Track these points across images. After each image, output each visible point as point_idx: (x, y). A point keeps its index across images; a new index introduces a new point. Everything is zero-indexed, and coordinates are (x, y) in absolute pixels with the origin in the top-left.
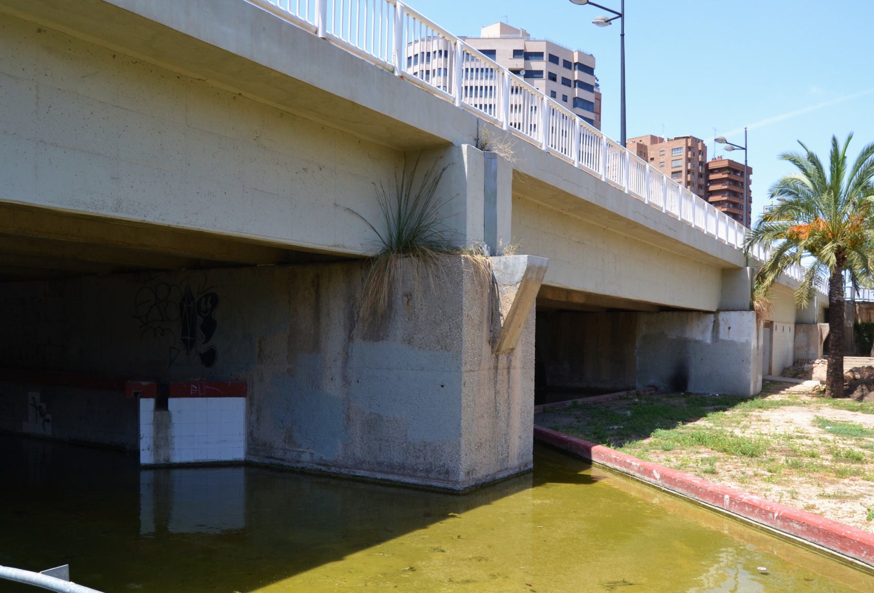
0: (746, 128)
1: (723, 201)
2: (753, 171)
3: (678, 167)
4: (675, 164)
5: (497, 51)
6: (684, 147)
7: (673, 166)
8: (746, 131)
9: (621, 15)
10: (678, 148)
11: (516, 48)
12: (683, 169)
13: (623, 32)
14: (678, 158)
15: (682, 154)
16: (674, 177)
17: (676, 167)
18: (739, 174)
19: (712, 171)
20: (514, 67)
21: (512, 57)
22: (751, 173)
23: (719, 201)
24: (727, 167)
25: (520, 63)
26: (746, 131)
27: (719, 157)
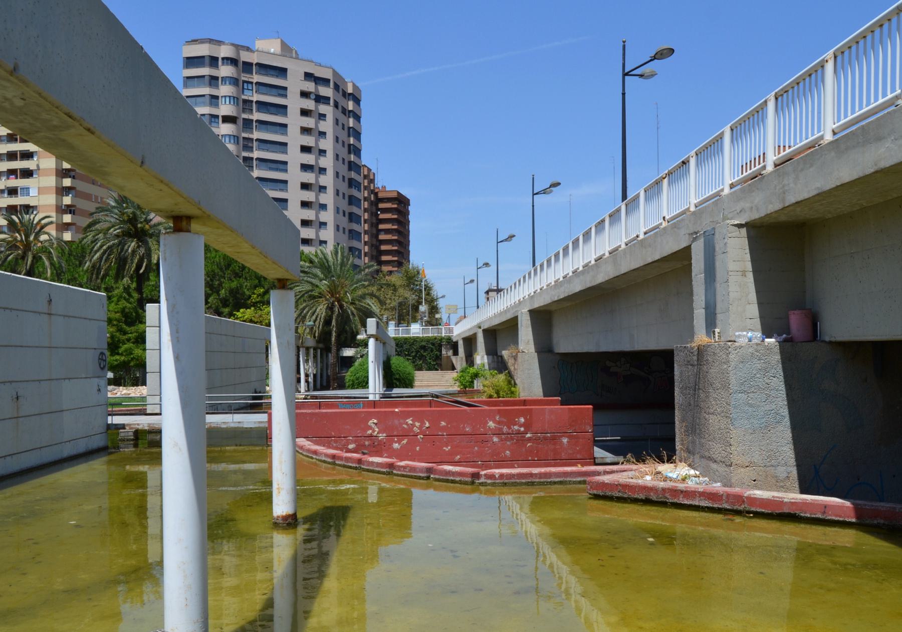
0: (533, 175)
1: (392, 229)
2: (411, 203)
5: (288, 70)
8: (533, 178)
9: (625, 74)
13: (624, 91)
18: (403, 205)
19: (382, 200)
20: (305, 89)
21: (303, 79)
22: (409, 205)
23: (389, 229)
25: (310, 86)
26: (533, 178)
27: (382, 186)
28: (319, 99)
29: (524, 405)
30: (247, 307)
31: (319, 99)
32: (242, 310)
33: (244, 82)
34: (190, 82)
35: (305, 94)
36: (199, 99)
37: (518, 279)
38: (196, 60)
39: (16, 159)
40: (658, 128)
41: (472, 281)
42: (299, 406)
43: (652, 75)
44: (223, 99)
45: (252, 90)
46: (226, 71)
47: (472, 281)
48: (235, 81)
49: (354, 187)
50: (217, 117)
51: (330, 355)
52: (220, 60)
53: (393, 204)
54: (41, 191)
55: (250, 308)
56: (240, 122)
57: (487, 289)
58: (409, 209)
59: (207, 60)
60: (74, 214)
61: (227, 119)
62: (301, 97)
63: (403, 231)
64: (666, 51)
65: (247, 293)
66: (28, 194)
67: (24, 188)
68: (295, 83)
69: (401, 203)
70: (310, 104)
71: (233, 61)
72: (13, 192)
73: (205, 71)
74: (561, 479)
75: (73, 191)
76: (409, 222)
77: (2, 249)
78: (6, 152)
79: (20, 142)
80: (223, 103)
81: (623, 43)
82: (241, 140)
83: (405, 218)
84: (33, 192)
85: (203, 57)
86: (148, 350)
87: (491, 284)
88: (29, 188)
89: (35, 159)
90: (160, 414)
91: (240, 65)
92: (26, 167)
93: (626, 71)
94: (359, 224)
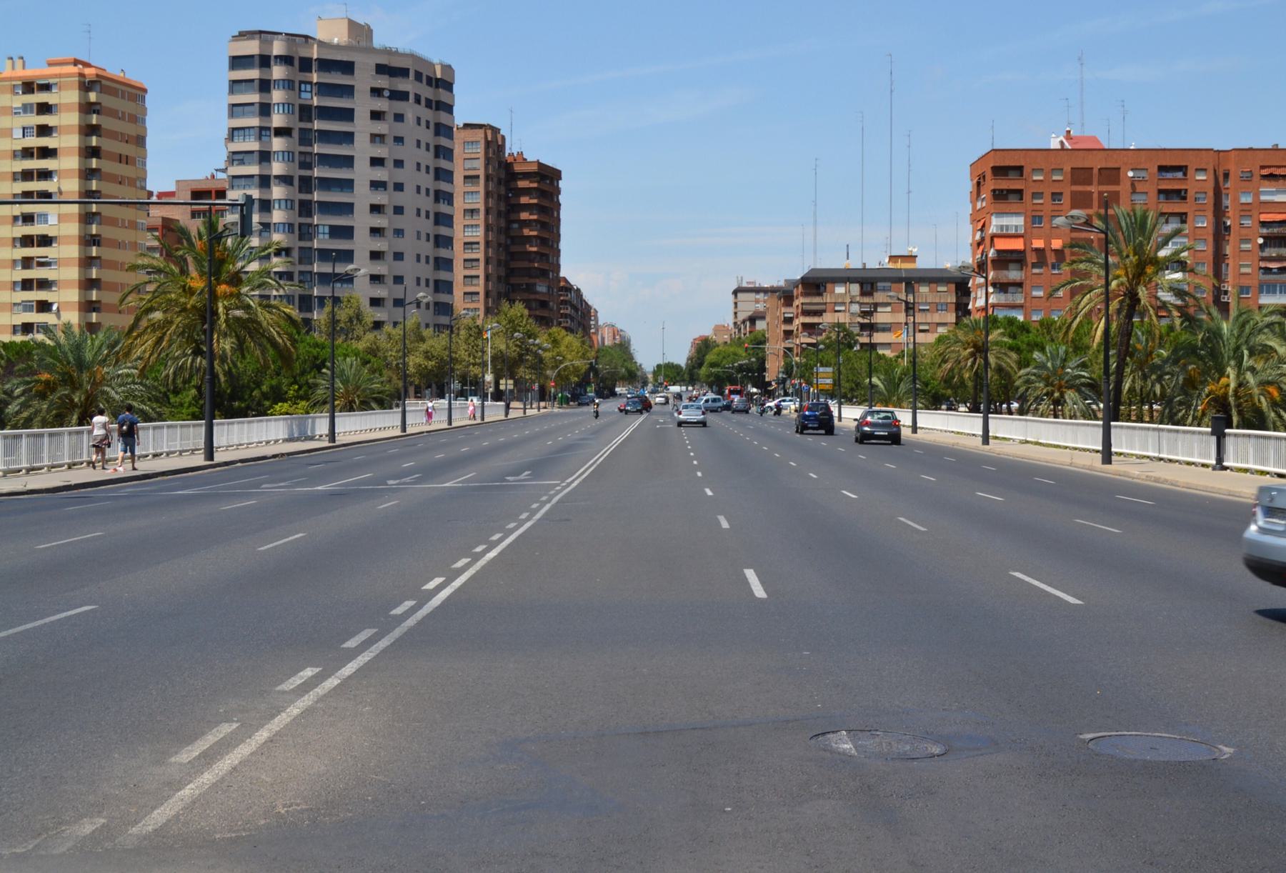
1: (530, 220)
3: (475, 169)
4: (468, 164)
5: (356, 66)
6: (483, 142)
7: (467, 167)
10: (472, 142)
11: (379, 62)
12: (481, 173)
14: (473, 156)
15: (479, 151)
16: (468, 183)
17: (469, 169)
22: (561, 179)
24: (535, 173)
25: (383, 82)
28: (400, 96)
30: (285, 401)
31: (400, 96)
32: (280, 404)
33: (301, 82)
34: (236, 87)
35: (376, 92)
36: (247, 108)
38: (243, 60)
39: (32, 179)
40: (891, 91)
44: (276, 107)
45: (311, 92)
46: (278, 72)
48: (288, 84)
49: (442, 201)
50: (269, 129)
52: (272, 58)
53: (531, 182)
54: (61, 218)
55: (286, 402)
56: (296, 134)
57: (735, 287)
58: (560, 186)
59: (257, 61)
60: (99, 245)
61: (280, 132)
62: (371, 96)
63: (548, 221)
65: (285, 389)
66: (46, 222)
67: (41, 215)
68: (364, 79)
69: (548, 178)
70: (381, 104)
71: (286, 60)
72: (28, 219)
73: (254, 74)
75: (97, 218)
76: (560, 205)
77: (1021, 871)
78: (20, 170)
79: (38, 158)
80: (276, 112)
82: (297, 155)
83: (552, 200)
84: (53, 220)
85: (252, 56)
87: (742, 278)
88: (47, 215)
89: (55, 180)
90: (465, 293)
91: (296, 63)
92: (44, 189)
94: (450, 248)
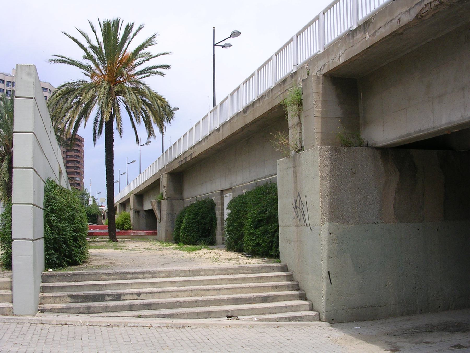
0: (214, 28)
8: (214, 30)
9: (215, 45)
26: (214, 30)
29: (89, 308)
37: (158, 158)
41: (124, 173)
42: (79, 173)
43: (230, 46)
47: (124, 173)
51: (109, 115)
64: (236, 33)
74: (193, 299)
81: (213, 29)
86: (16, 168)
93: (215, 43)
